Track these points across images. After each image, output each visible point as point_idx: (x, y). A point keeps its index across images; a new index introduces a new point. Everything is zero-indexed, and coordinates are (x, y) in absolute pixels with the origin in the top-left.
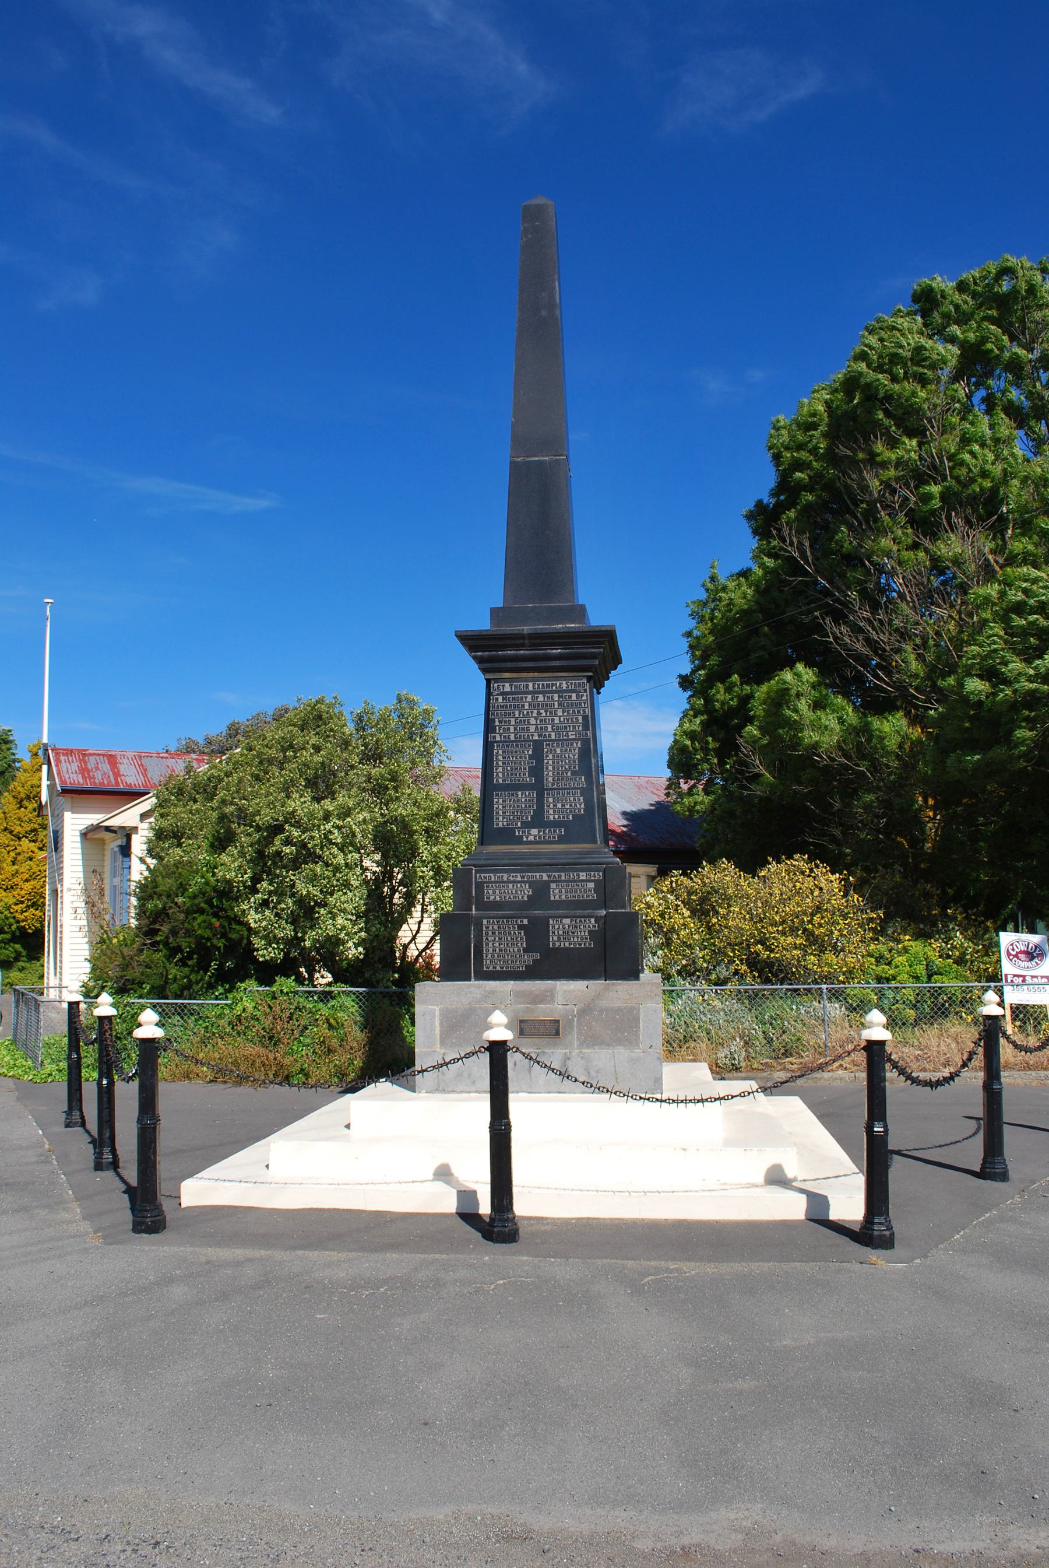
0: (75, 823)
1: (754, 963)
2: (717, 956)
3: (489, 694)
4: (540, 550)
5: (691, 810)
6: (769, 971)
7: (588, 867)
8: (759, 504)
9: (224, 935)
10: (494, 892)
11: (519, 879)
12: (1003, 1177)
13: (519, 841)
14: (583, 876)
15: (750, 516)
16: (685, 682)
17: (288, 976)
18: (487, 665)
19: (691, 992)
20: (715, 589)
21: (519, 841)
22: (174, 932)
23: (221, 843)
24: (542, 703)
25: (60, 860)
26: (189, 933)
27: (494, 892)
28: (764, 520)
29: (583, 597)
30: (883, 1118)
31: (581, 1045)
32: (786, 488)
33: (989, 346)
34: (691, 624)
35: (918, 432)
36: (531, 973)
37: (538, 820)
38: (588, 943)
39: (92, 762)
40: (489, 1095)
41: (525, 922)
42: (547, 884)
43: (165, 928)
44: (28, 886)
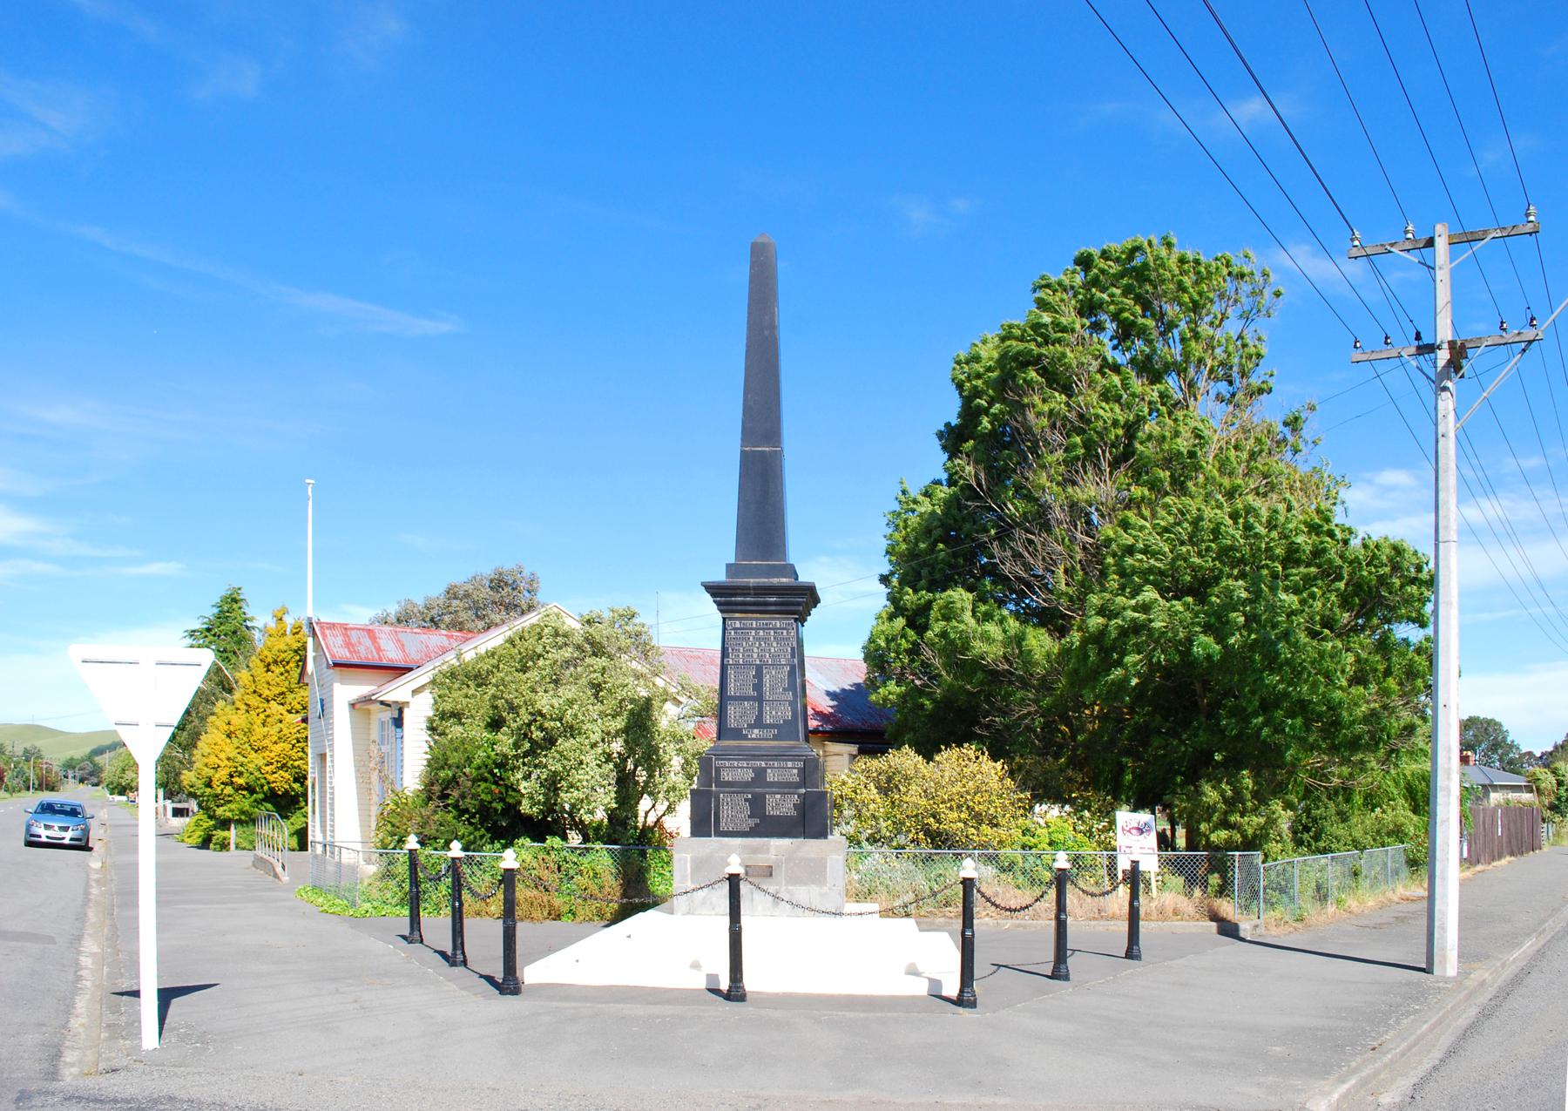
0: (345, 692)
1: (928, 832)
2: (898, 827)
3: (724, 629)
4: (762, 518)
5: (885, 699)
6: (939, 839)
7: (794, 758)
8: (948, 425)
9: (502, 800)
12: (1066, 978)
13: (745, 738)
14: (790, 764)
15: (940, 435)
16: (884, 579)
17: (994, 758)
18: (724, 607)
19: (876, 857)
20: (909, 504)
21: (745, 738)
22: (463, 796)
23: (496, 724)
24: (763, 637)
25: (330, 726)
26: (475, 796)
28: (953, 439)
29: (793, 557)
30: (972, 926)
31: (788, 883)
32: (970, 414)
33: (1126, 315)
34: (889, 531)
35: (1067, 389)
36: (753, 833)
37: (759, 723)
38: (793, 813)
39: (354, 636)
42: (764, 770)
43: (456, 794)
44: (277, 748)
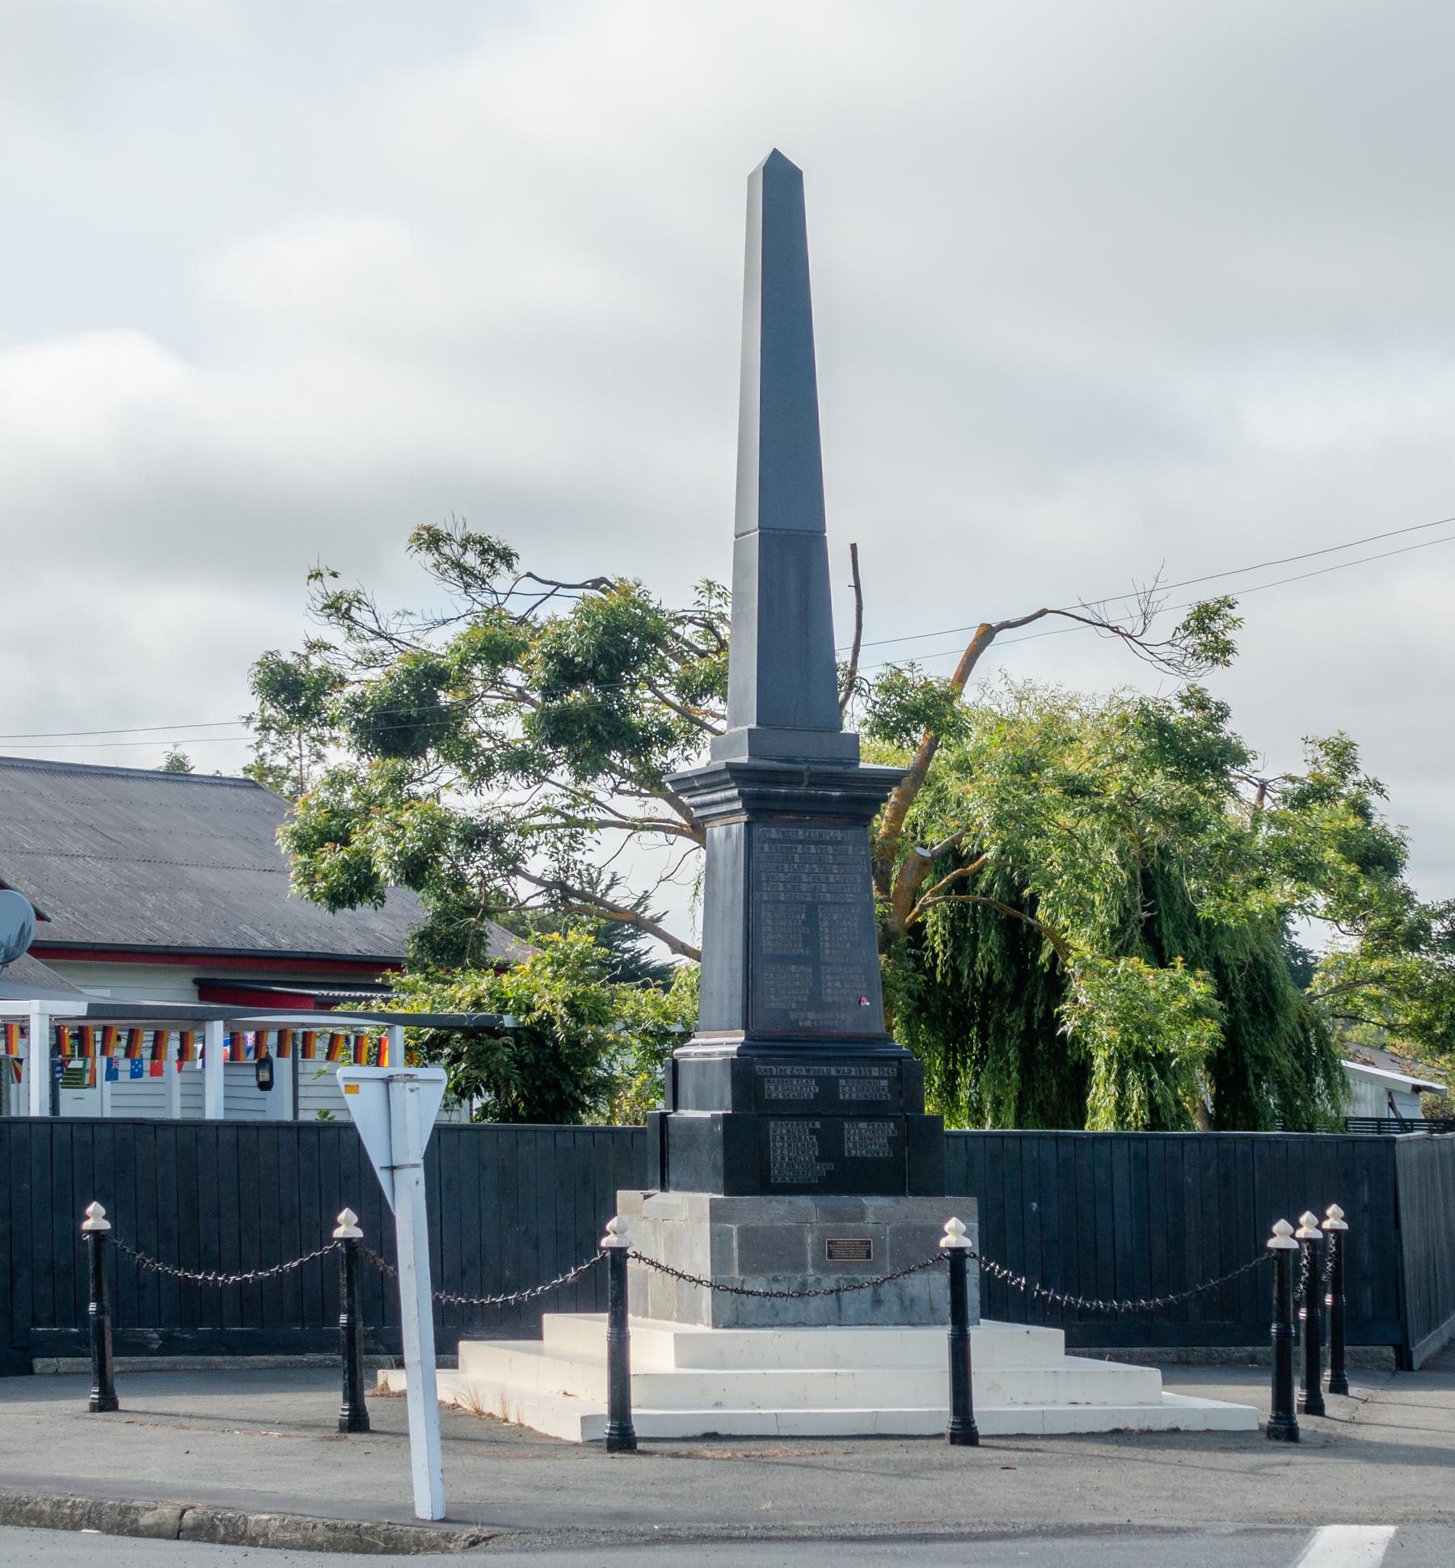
10: (776, 1089)
11: (804, 1073)
14: (875, 1072)
27: (776, 1089)
40: (633, 1370)
41: (818, 1125)
42: (836, 1079)
